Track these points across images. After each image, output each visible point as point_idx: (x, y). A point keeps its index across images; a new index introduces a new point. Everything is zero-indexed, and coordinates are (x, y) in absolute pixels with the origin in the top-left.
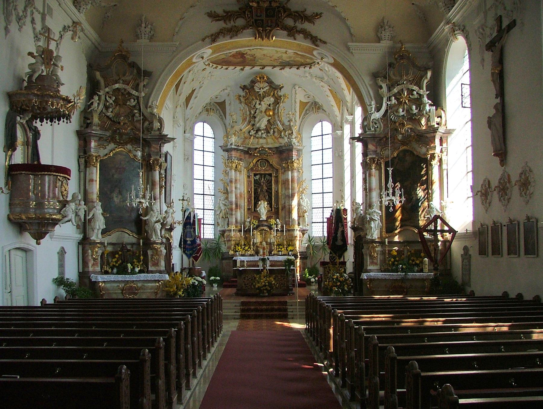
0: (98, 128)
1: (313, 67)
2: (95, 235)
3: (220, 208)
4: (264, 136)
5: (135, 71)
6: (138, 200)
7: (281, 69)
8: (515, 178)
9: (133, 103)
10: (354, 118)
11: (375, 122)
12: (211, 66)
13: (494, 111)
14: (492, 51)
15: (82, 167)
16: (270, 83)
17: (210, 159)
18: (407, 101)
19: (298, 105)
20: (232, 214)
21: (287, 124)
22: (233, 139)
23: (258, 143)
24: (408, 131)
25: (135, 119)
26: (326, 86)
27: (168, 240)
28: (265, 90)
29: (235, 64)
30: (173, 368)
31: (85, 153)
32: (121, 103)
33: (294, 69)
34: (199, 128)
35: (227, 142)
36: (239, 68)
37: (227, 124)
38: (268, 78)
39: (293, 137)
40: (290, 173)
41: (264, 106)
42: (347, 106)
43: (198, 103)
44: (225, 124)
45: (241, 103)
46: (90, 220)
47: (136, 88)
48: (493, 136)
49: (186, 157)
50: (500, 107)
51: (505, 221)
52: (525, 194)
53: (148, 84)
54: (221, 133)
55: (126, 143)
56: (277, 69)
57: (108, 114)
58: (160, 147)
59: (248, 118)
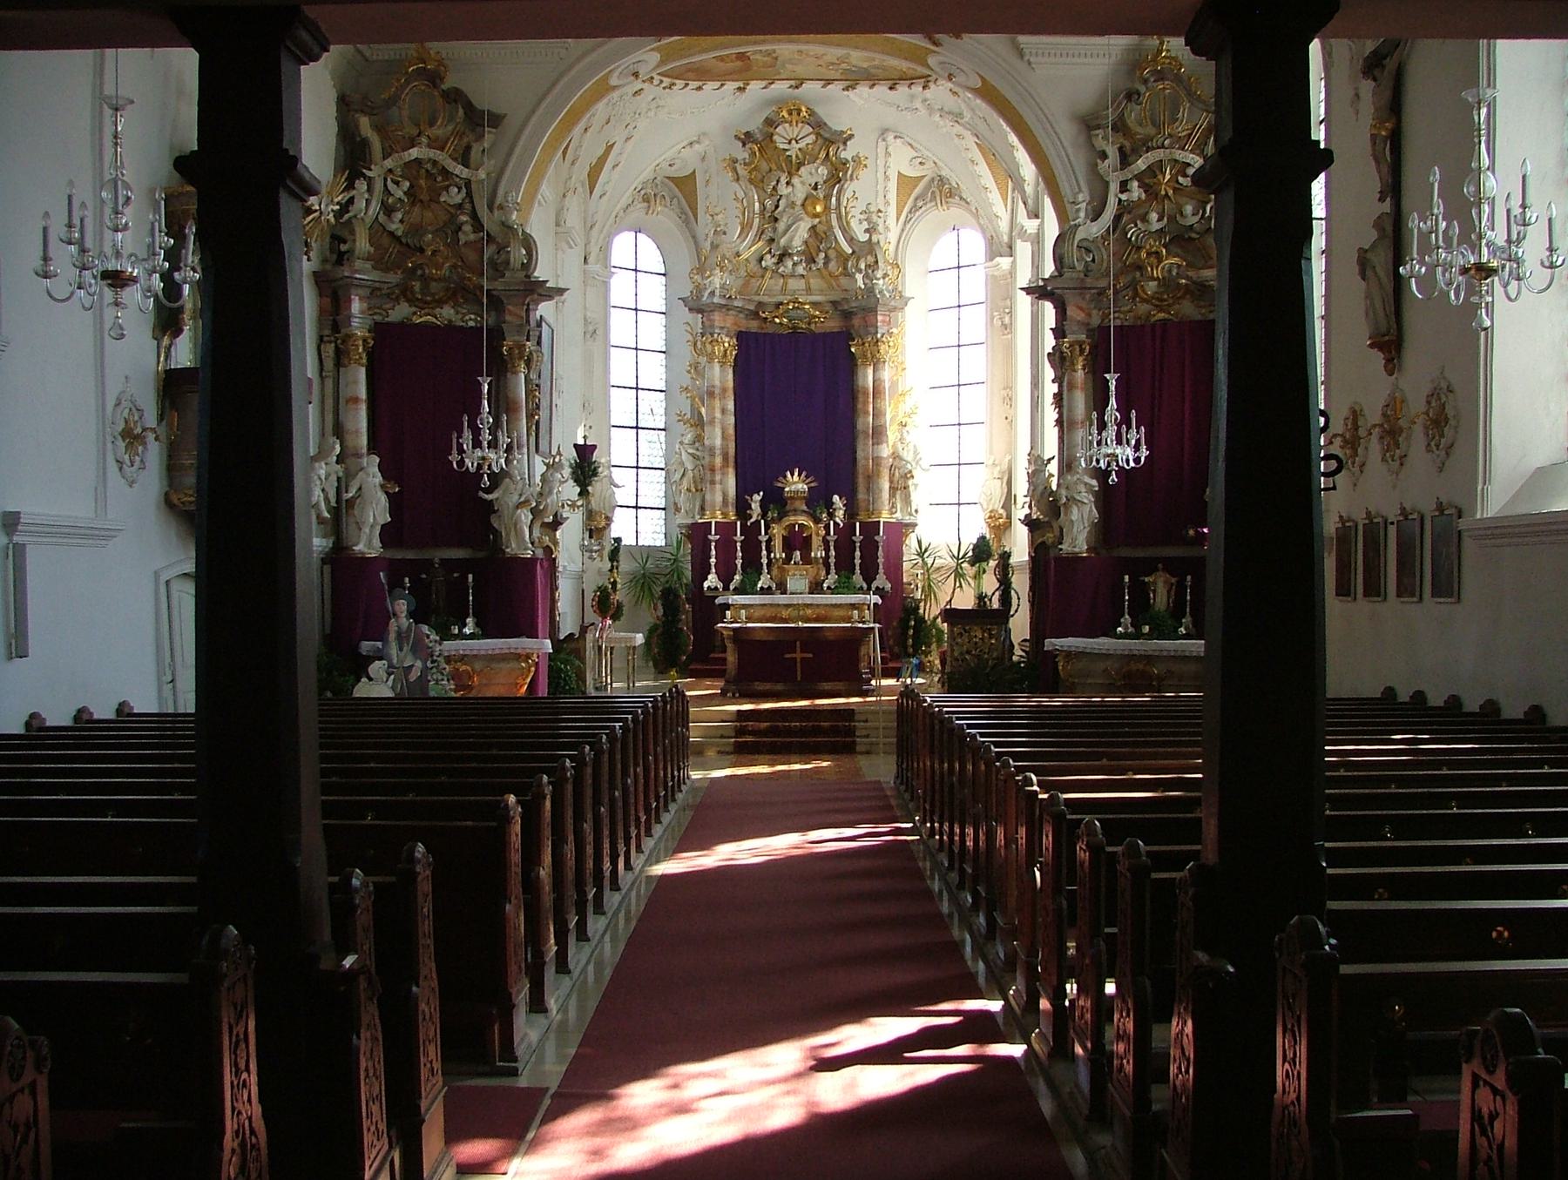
0: (368, 265)
1: (931, 85)
2: (364, 538)
3: (682, 463)
4: (800, 270)
5: (461, 111)
6: (478, 453)
7: (846, 89)
8: (1416, 404)
9: (455, 196)
10: (1041, 227)
11: (1085, 248)
12: (656, 82)
13: (1374, 235)
14: (1375, 80)
15: (329, 364)
16: (818, 125)
17: (654, 332)
18: (1171, 192)
19: (893, 185)
20: (713, 482)
21: (863, 237)
22: (717, 280)
23: (783, 291)
24: (1170, 271)
25: (463, 238)
26: (967, 134)
27: (548, 551)
28: (802, 144)
29: (722, 77)
30: (587, 827)
31: (336, 328)
32: (425, 197)
33: (882, 90)
34: (623, 247)
35: (699, 289)
36: (731, 86)
37: (701, 237)
38: (812, 113)
39: (879, 274)
40: (870, 371)
41: (799, 190)
42: (1023, 192)
43: (621, 181)
44: (694, 237)
45: (738, 180)
46: (351, 503)
47: (464, 159)
48: (1368, 296)
49: (591, 328)
50: (1389, 229)
51: (1393, 514)
52: (1437, 446)
53: (493, 145)
54: (686, 262)
55: (440, 303)
56: (836, 88)
57: (393, 227)
58: (528, 310)
59: (757, 221)
